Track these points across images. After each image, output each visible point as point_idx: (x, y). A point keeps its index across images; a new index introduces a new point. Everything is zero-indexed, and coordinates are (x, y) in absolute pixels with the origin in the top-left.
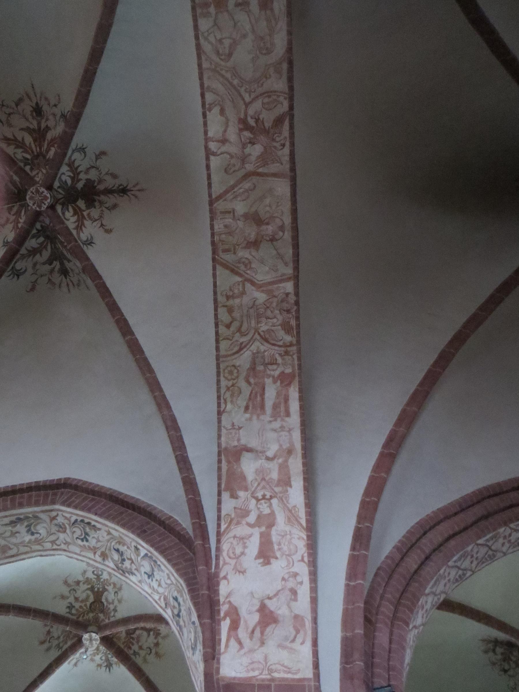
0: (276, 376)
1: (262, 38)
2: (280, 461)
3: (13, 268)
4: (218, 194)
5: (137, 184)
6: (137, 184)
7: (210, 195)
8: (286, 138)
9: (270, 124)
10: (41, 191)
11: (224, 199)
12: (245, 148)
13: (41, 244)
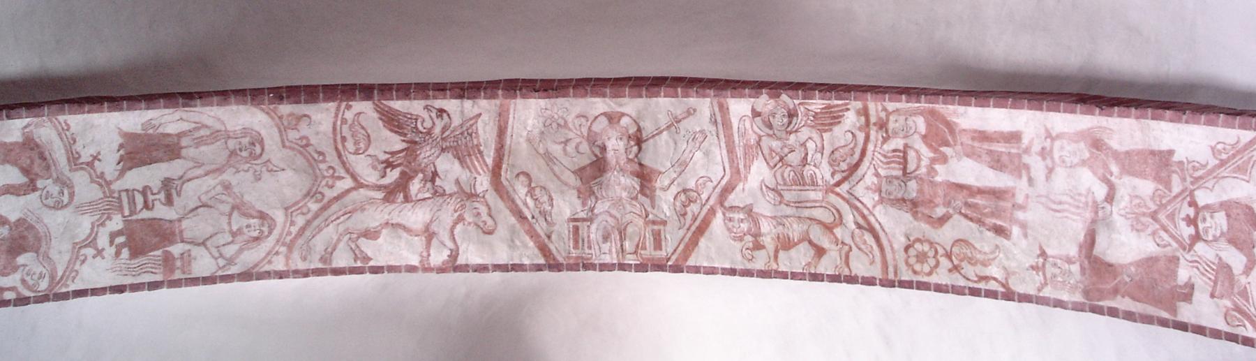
0: (932, 155)
1: (233, 153)
2: (1114, 168)
4: (536, 251)
7: (539, 268)
8: (426, 107)
9: (397, 138)
11: (546, 240)
12: (444, 190)
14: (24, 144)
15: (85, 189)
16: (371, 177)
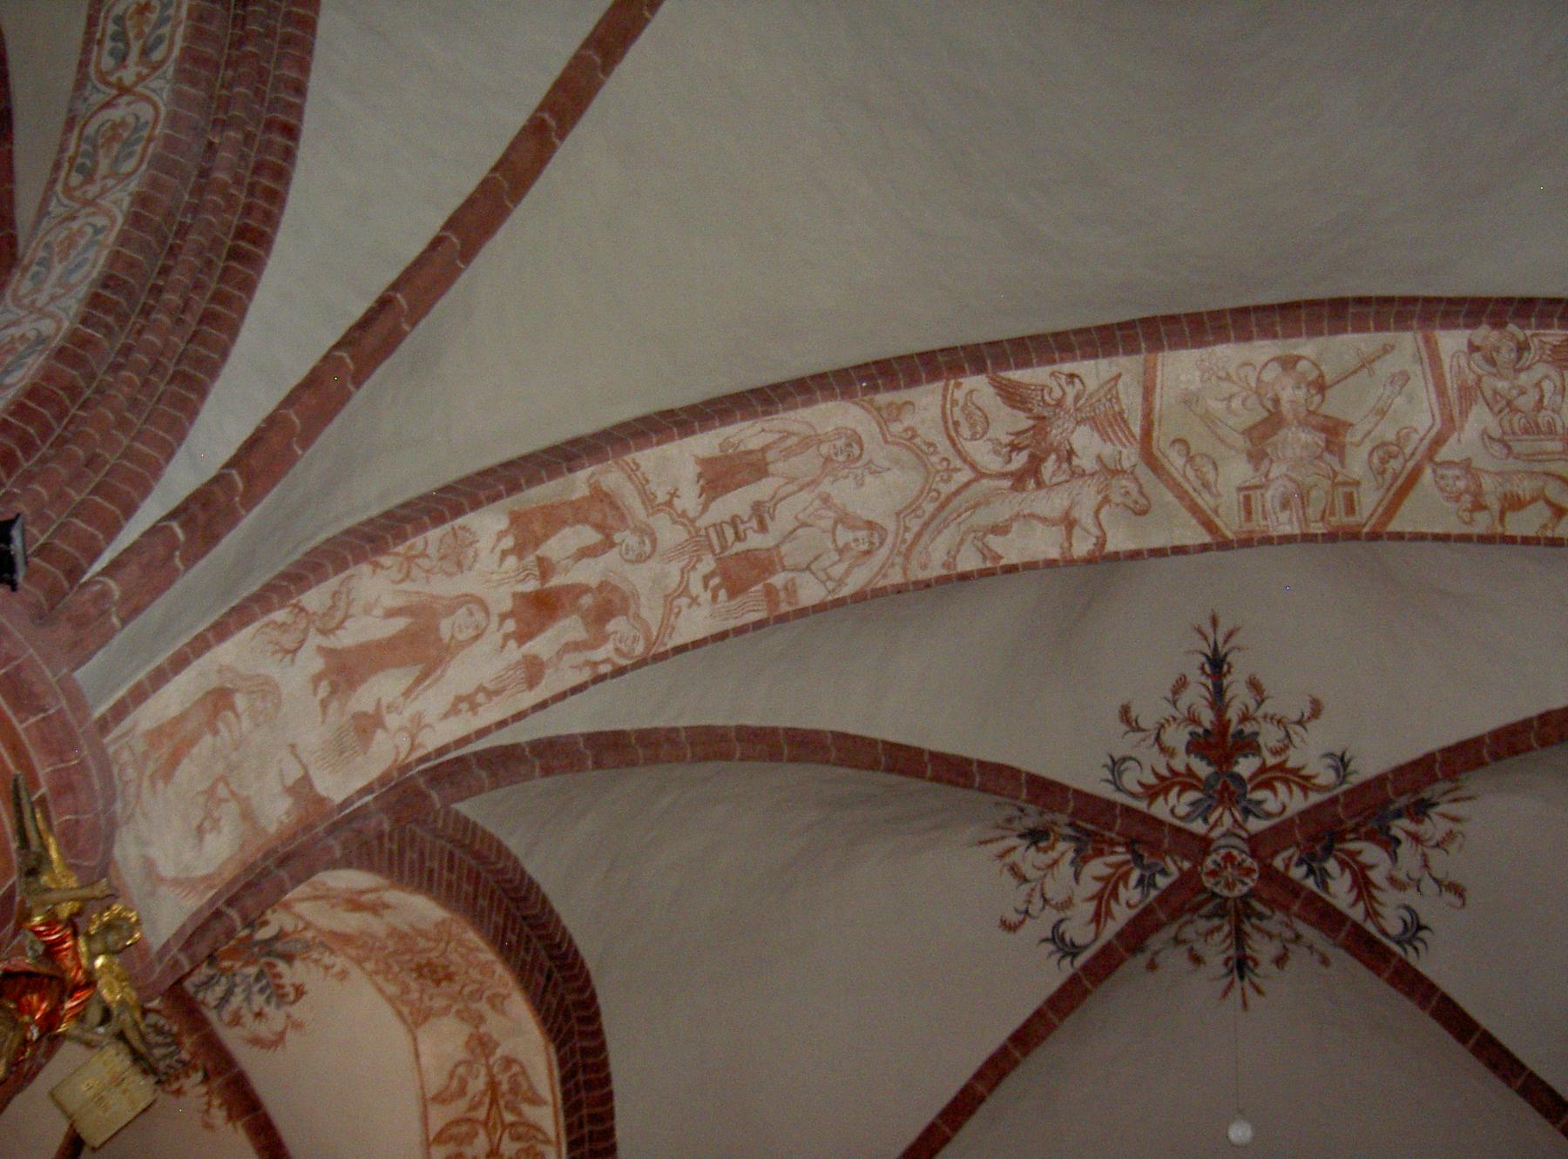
1: (828, 460)
3: (1399, 942)
5: (1200, 631)
6: (1200, 631)
9: (1022, 415)
10: (1212, 867)
12: (1084, 471)
13: (1343, 865)
14: (592, 496)
15: (670, 534)
16: (992, 463)
